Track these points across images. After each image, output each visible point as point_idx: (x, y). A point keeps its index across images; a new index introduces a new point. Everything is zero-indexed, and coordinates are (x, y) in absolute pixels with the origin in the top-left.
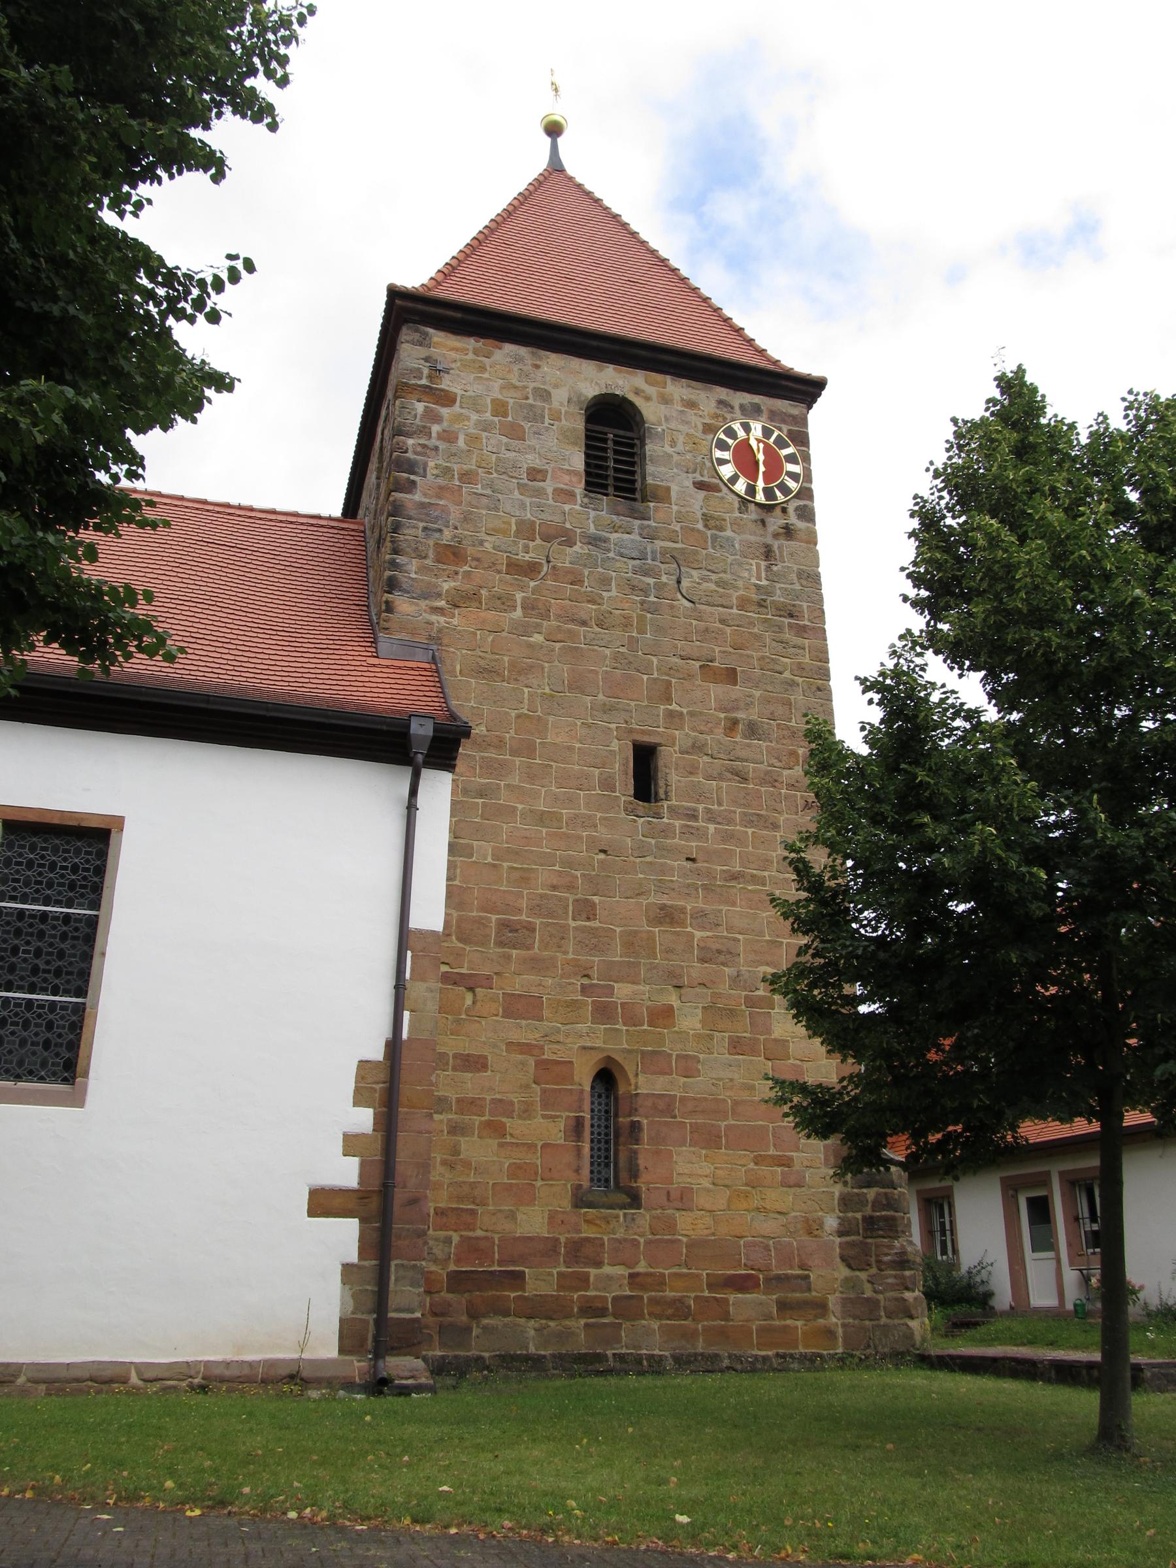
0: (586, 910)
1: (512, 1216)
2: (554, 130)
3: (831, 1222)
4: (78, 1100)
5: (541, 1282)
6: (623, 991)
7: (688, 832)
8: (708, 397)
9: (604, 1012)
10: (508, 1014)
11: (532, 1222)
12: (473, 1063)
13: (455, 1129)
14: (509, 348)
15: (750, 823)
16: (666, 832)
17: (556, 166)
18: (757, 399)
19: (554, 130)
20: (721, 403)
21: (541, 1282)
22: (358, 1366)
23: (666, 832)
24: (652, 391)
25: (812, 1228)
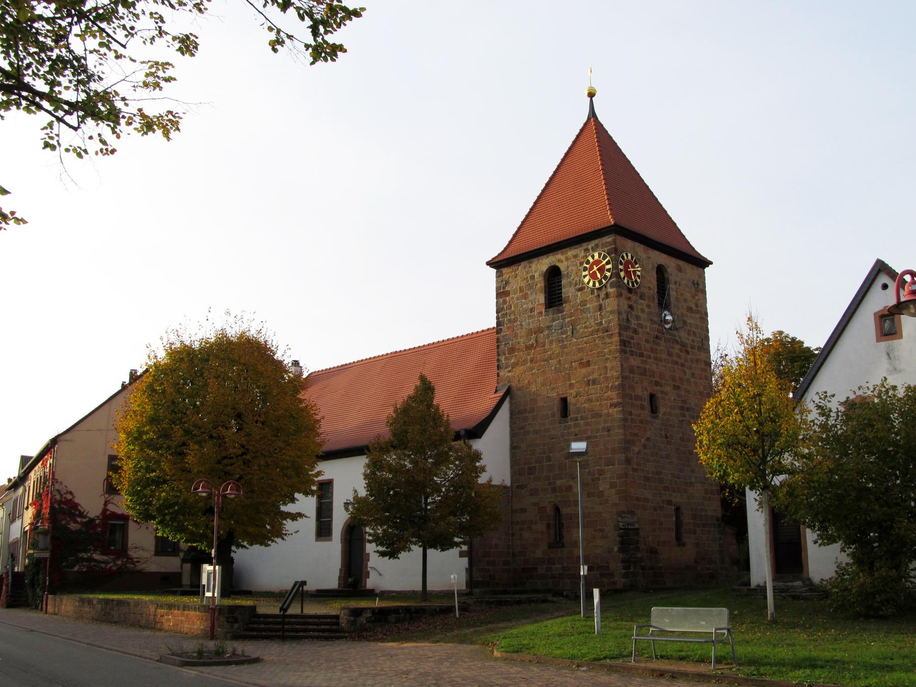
0: (549, 459)
1: (534, 552)
2: (591, 95)
3: (616, 549)
4: (331, 540)
5: (541, 570)
6: (558, 482)
7: (576, 426)
8: (578, 251)
9: (554, 490)
10: (531, 495)
11: (539, 553)
12: (524, 510)
13: (521, 529)
14: (523, 264)
15: (593, 417)
16: (569, 427)
17: (592, 114)
18: (596, 241)
19: (591, 95)
20: (82, 601)
21: (541, 570)
22: (469, 590)
23: (569, 427)
24: (563, 257)
25: (610, 551)
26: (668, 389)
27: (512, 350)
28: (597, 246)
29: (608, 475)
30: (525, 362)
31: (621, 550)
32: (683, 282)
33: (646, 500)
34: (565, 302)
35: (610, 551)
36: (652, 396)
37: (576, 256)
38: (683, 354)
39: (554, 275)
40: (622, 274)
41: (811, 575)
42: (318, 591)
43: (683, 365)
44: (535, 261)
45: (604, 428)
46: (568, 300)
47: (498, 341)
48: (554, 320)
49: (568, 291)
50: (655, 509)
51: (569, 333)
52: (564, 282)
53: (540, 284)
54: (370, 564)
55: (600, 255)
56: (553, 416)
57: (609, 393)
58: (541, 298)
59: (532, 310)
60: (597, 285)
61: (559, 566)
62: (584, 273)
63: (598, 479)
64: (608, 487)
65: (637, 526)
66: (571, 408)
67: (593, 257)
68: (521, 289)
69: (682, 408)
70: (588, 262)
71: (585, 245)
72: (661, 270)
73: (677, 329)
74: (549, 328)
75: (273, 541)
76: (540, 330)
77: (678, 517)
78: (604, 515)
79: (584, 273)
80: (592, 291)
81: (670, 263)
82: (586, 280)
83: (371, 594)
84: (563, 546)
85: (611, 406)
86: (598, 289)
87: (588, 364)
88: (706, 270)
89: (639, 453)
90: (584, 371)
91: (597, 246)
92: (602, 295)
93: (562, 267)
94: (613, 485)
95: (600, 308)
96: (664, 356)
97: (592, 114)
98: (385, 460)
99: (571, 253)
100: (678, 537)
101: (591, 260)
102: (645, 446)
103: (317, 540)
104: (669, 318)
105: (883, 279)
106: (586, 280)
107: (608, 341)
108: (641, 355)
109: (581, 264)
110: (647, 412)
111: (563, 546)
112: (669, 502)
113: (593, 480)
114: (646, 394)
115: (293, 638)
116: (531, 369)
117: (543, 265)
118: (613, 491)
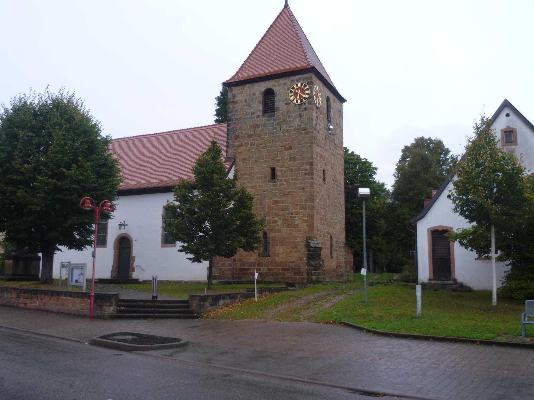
1: (249, 259)
3: (305, 259)
4: (106, 247)
7: (281, 185)
8: (287, 81)
14: (247, 85)
15: (293, 180)
17: (286, 6)
24: (276, 84)
25: (301, 260)
26: (329, 168)
27: (237, 137)
28: (300, 79)
29: (301, 215)
30: (247, 144)
31: (308, 259)
32: (335, 109)
33: (321, 231)
34: (277, 111)
35: (301, 260)
36: (324, 171)
37: (285, 84)
38: (334, 149)
39: (269, 94)
40: (315, 97)
41: (456, 277)
42: (99, 279)
43: (334, 156)
44: (256, 84)
45: (300, 188)
46: (278, 109)
47: (228, 130)
48: (268, 120)
49: (279, 103)
50: (323, 237)
51: (279, 129)
52: (276, 98)
53: (261, 98)
54: (135, 263)
55: (302, 84)
56: (265, 177)
57: (304, 166)
58: (261, 107)
59: (253, 114)
60: (299, 102)
61: (266, 268)
62: (290, 95)
63: (295, 217)
64: (301, 221)
65: (320, 246)
66: (278, 173)
67: (297, 85)
68: (246, 101)
69: (334, 180)
70: (293, 88)
71: (292, 78)
72: (328, 99)
73: (333, 135)
74: (264, 125)
75: (85, 247)
76: (257, 126)
77: (331, 242)
78: (298, 238)
79: (290, 95)
80: (296, 105)
81: (332, 97)
82: (292, 98)
83: (136, 281)
84: (269, 256)
85: (306, 174)
86: (299, 104)
87: (291, 148)
88: (343, 104)
89: (318, 203)
90: (287, 152)
91: (300, 79)
92: (303, 107)
93: (276, 90)
94: (305, 221)
95: (301, 116)
96: (328, 149)
97: (286, 6)
98: (189, 196)
99: (282, 81)
100: (331, 254)
101: (296, 87)
102: (321, 199)
103: (162, 246)
104: (331, 127)
105: (506, 111)
106: (292, 98)
107: (304, 135)
108: (320, 147)
109: (289, 89)
110: (322, 180)
111: (269, 256)
112: (328, 233)
113: (291, 217)
114: (322, 170)
115: (155, 318)
116: (250, 149)
117: (263, 86)
118: (305, 224)
